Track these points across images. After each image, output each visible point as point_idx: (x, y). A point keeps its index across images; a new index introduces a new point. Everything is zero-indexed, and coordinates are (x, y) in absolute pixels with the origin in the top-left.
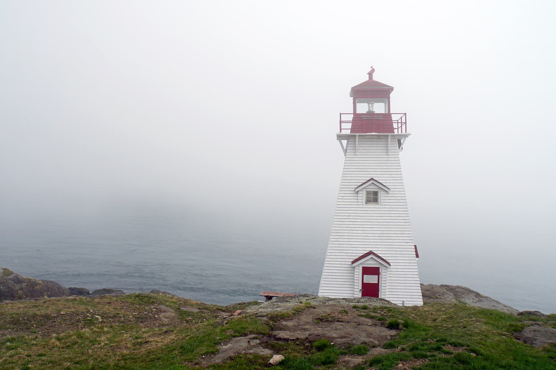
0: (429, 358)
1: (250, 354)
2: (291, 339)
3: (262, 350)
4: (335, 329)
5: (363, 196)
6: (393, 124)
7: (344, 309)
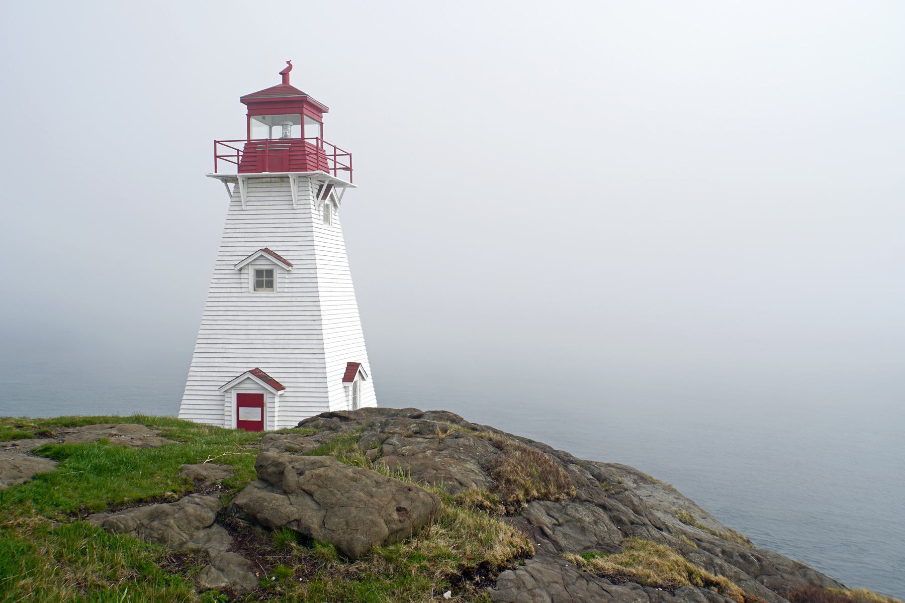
5: (250, 277)
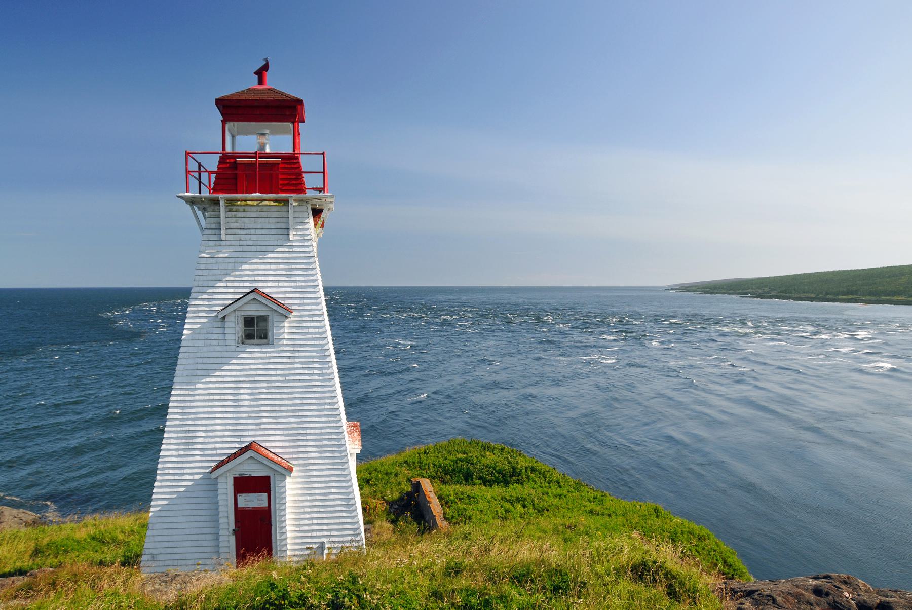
5: (235, 328)
6: (304, 175)
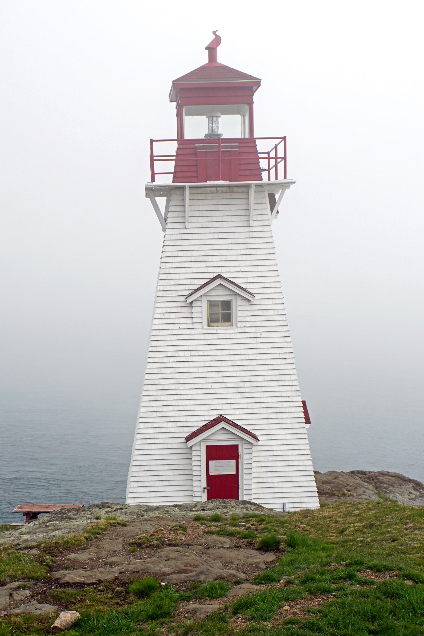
0: (334, 594)
1: (17, 615)
2: (87, 582)
3: (37, 607)
4: (166, 558)
6: (260, 160)
7: (177, 523)
